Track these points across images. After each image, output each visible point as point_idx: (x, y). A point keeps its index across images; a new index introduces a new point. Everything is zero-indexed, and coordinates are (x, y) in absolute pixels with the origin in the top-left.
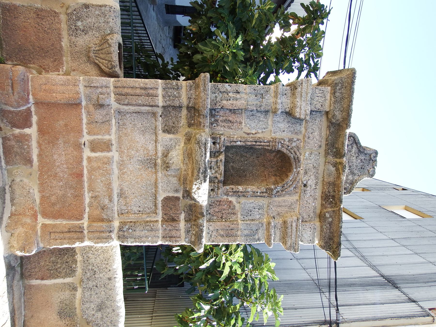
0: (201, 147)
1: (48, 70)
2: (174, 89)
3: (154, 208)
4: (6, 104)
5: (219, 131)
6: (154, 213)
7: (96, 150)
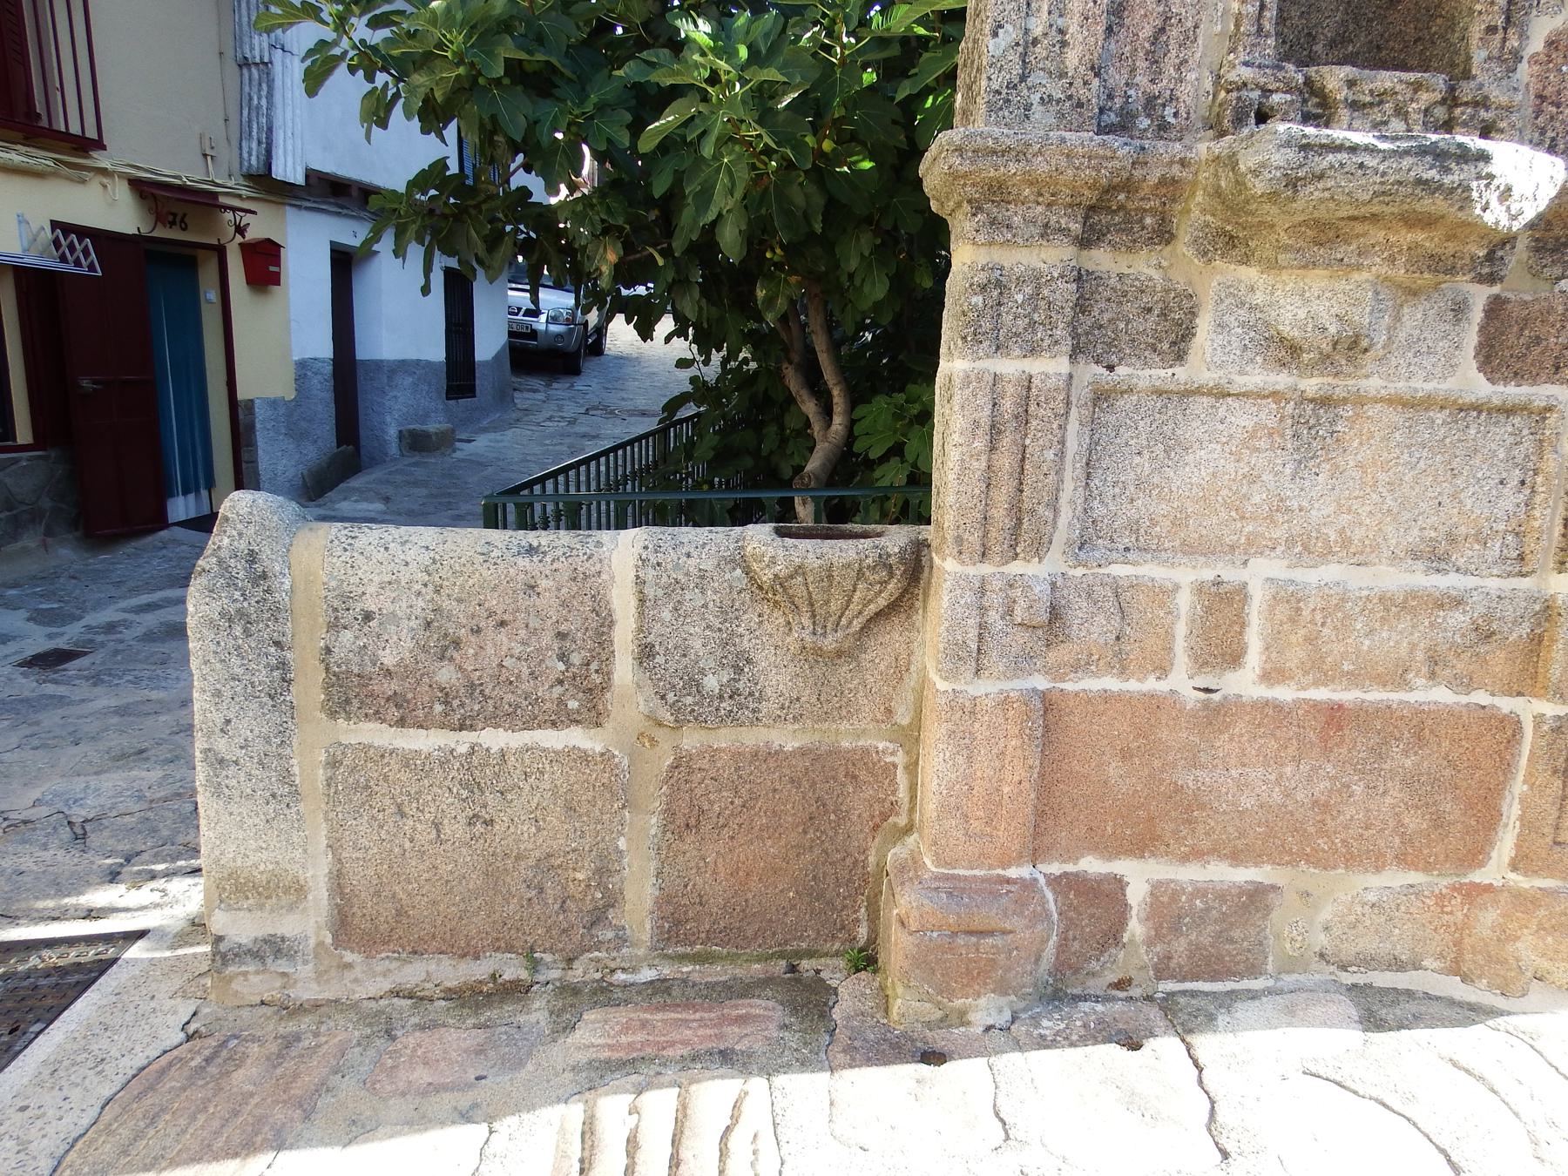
0: (1318, 170)
1: (887, 805)
2: (999, 304)
3: (1517, 420)
4: (1038, 960)
5: (1201, 92)
6: (1545, 418)
7: (1234, 646)
